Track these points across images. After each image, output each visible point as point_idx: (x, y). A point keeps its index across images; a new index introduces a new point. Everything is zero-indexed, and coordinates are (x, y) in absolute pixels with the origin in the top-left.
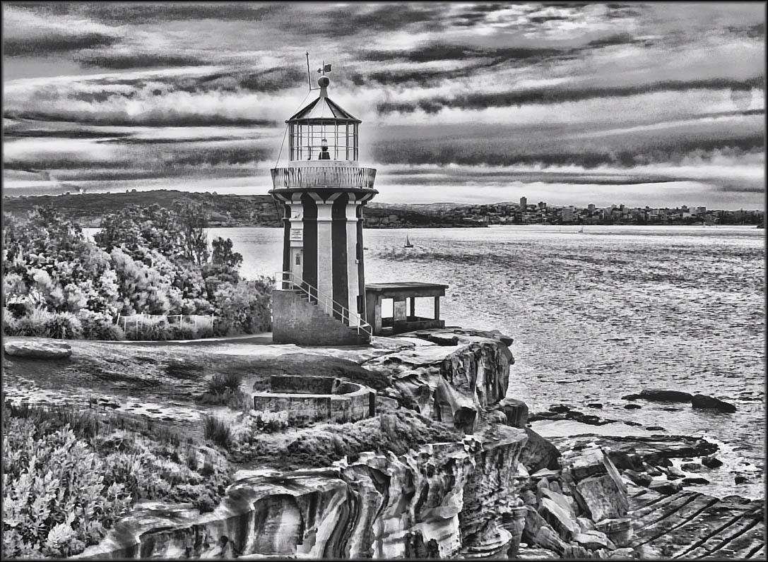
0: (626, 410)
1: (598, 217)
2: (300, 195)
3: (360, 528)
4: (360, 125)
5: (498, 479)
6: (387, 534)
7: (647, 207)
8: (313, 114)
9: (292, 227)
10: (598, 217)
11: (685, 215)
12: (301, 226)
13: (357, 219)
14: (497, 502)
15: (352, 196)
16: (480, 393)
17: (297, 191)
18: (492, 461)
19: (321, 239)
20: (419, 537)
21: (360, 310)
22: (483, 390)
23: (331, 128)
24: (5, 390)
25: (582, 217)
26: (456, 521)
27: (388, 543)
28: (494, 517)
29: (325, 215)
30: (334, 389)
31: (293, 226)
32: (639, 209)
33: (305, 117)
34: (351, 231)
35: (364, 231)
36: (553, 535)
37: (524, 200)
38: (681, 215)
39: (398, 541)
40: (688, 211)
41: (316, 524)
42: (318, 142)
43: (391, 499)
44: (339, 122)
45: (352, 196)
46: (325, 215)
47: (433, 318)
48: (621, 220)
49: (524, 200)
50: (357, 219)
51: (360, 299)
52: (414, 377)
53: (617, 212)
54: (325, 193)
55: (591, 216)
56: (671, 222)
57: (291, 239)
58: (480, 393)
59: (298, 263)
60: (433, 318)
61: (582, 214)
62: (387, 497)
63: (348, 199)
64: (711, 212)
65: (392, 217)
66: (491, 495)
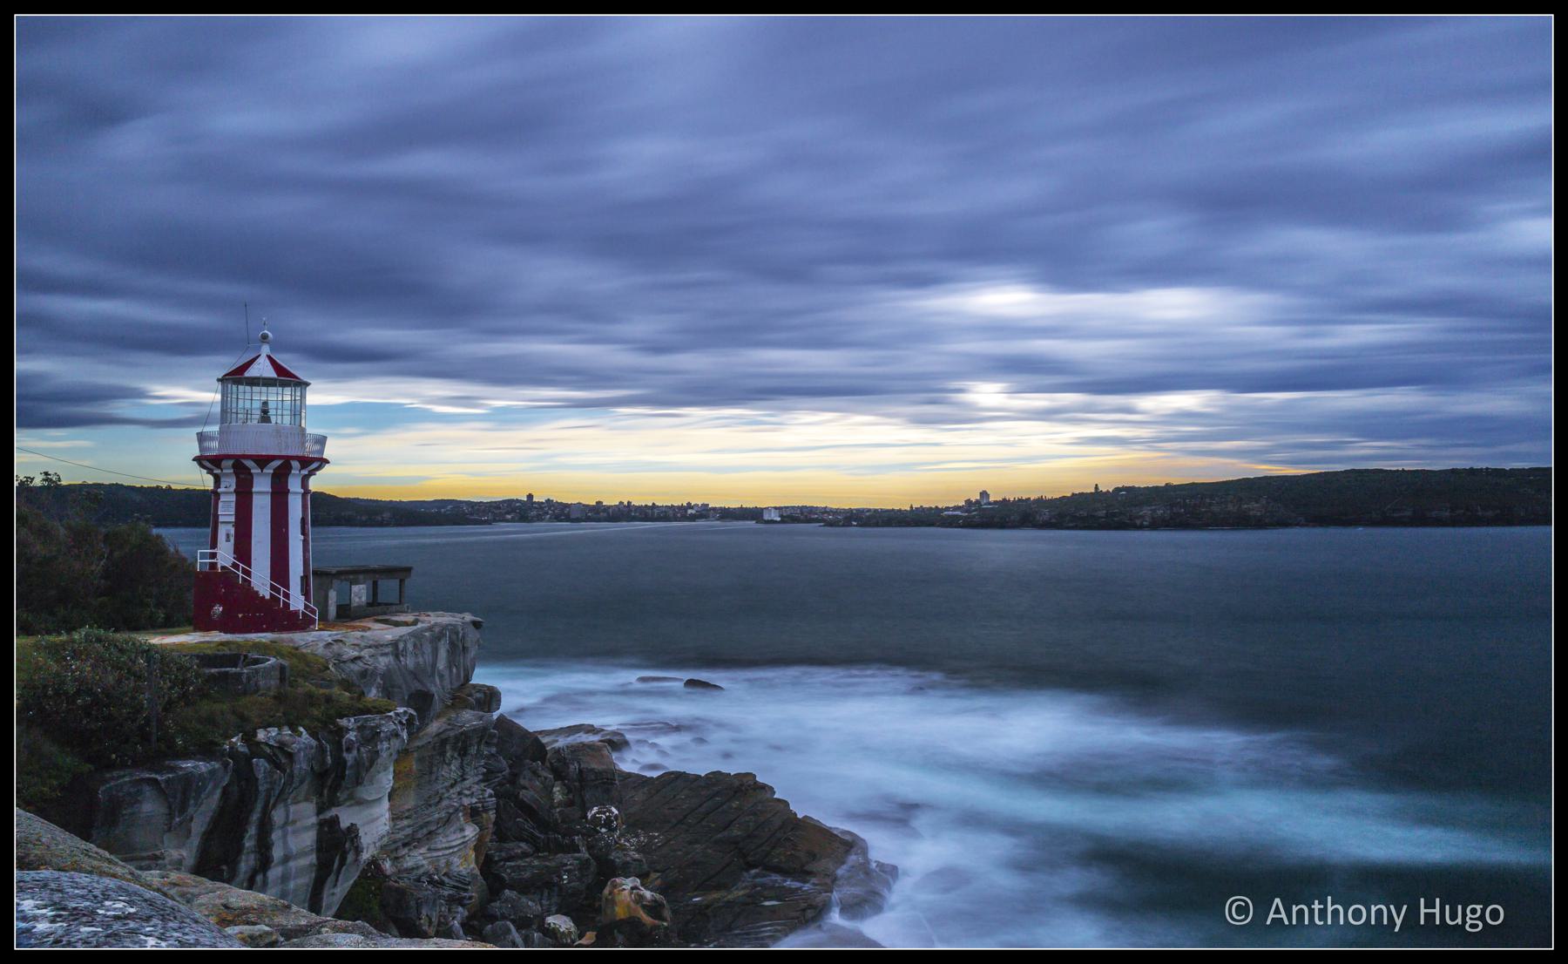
2: (230, 462)
3: (255, 817)
5: (462, 767)
6: (294, 822)
8: (252, 372)
12: (233, 498)
14: (460, 793)
15: (295, 464)
16: (441, 677)
17: (228, 457)
18: (454, 749)
19: (942, 940)
20: (335, 821)
21: (305, 592)
22: (446, 673)
26: (386, 804)
27: (294, 832)
28: (457, 810)
29: (262, 486)
31: (223, 498)
33: (247, 374)
36: (528, 826)
37: (530, 496)
39: (307, 829)
41: (191, 810)
42: (257, 405)
43: (296, 780)
44: (284, 385)
45: (295, 464)
46: (262, 486)
49: (530, 496)
51: (305, 579)
52: (359, 658)
54: (263, 461)
58: (441, 677)
59: (228, 540)
62: (291, 776)
63: (290, 468)
66: (452, 786)
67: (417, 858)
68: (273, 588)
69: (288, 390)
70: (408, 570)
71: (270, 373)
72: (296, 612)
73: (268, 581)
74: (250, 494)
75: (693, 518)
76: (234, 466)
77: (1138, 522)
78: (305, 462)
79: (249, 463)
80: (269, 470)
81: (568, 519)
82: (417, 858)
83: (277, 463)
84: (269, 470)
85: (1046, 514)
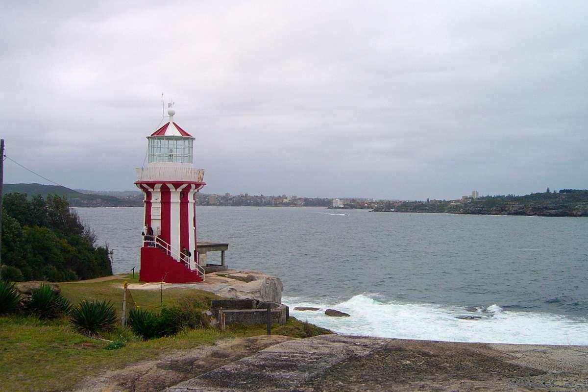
0: (350, 314)
1: (231, 202)
2: (161, 185)
4: (194, 141)
7: (262, 195)
9: (152, 206)
10: (231, 202)
11: (285, 201)
12: (160, 205)
13: (194, 201)
23: (179, 142)
24: (586, 263)
25: (222, 201)
29: (175, 198)
30: (255, 306)
32: (257, 196)
34: (190, 208)
35: (196, 207)
38: (283, 201)
40: (286, 198)
44: (185, 139)
45: (193, 186)
46: (175, 198)
47: (221, 264)
48: (246, 204)
50: (194, 201)
53: (243, 198)
54: (177, 185)
55: (227, 200)
56: (276, 205)
57: (151, 214)
60: (221, 264)
61: (222, 199)
64: (300, 199)
65: (99, 200)
67: (82, 327)
68: (182, 256)
69: (187, 142)
70: (227, 245)
71: (178, 134)
72: (195, 271)
73: (179, 252)
74: (169, 203)
75: (287, 205)
76: (162, 188)
77: (575, 212)
78: (198, 185)
79: (170, 186)
80: (180, 190)
81: (208, 204)
82: (82, 327)
83: (184, 186)
84: (180, 190)
85: (517, 206)
